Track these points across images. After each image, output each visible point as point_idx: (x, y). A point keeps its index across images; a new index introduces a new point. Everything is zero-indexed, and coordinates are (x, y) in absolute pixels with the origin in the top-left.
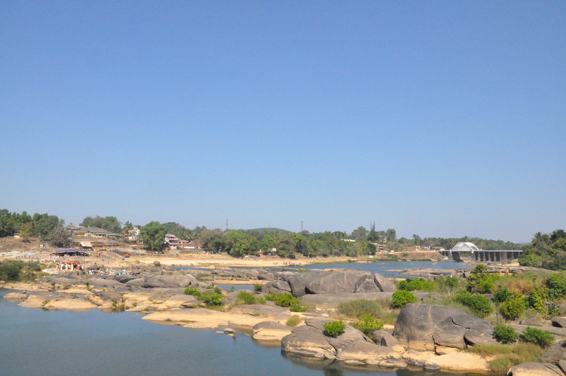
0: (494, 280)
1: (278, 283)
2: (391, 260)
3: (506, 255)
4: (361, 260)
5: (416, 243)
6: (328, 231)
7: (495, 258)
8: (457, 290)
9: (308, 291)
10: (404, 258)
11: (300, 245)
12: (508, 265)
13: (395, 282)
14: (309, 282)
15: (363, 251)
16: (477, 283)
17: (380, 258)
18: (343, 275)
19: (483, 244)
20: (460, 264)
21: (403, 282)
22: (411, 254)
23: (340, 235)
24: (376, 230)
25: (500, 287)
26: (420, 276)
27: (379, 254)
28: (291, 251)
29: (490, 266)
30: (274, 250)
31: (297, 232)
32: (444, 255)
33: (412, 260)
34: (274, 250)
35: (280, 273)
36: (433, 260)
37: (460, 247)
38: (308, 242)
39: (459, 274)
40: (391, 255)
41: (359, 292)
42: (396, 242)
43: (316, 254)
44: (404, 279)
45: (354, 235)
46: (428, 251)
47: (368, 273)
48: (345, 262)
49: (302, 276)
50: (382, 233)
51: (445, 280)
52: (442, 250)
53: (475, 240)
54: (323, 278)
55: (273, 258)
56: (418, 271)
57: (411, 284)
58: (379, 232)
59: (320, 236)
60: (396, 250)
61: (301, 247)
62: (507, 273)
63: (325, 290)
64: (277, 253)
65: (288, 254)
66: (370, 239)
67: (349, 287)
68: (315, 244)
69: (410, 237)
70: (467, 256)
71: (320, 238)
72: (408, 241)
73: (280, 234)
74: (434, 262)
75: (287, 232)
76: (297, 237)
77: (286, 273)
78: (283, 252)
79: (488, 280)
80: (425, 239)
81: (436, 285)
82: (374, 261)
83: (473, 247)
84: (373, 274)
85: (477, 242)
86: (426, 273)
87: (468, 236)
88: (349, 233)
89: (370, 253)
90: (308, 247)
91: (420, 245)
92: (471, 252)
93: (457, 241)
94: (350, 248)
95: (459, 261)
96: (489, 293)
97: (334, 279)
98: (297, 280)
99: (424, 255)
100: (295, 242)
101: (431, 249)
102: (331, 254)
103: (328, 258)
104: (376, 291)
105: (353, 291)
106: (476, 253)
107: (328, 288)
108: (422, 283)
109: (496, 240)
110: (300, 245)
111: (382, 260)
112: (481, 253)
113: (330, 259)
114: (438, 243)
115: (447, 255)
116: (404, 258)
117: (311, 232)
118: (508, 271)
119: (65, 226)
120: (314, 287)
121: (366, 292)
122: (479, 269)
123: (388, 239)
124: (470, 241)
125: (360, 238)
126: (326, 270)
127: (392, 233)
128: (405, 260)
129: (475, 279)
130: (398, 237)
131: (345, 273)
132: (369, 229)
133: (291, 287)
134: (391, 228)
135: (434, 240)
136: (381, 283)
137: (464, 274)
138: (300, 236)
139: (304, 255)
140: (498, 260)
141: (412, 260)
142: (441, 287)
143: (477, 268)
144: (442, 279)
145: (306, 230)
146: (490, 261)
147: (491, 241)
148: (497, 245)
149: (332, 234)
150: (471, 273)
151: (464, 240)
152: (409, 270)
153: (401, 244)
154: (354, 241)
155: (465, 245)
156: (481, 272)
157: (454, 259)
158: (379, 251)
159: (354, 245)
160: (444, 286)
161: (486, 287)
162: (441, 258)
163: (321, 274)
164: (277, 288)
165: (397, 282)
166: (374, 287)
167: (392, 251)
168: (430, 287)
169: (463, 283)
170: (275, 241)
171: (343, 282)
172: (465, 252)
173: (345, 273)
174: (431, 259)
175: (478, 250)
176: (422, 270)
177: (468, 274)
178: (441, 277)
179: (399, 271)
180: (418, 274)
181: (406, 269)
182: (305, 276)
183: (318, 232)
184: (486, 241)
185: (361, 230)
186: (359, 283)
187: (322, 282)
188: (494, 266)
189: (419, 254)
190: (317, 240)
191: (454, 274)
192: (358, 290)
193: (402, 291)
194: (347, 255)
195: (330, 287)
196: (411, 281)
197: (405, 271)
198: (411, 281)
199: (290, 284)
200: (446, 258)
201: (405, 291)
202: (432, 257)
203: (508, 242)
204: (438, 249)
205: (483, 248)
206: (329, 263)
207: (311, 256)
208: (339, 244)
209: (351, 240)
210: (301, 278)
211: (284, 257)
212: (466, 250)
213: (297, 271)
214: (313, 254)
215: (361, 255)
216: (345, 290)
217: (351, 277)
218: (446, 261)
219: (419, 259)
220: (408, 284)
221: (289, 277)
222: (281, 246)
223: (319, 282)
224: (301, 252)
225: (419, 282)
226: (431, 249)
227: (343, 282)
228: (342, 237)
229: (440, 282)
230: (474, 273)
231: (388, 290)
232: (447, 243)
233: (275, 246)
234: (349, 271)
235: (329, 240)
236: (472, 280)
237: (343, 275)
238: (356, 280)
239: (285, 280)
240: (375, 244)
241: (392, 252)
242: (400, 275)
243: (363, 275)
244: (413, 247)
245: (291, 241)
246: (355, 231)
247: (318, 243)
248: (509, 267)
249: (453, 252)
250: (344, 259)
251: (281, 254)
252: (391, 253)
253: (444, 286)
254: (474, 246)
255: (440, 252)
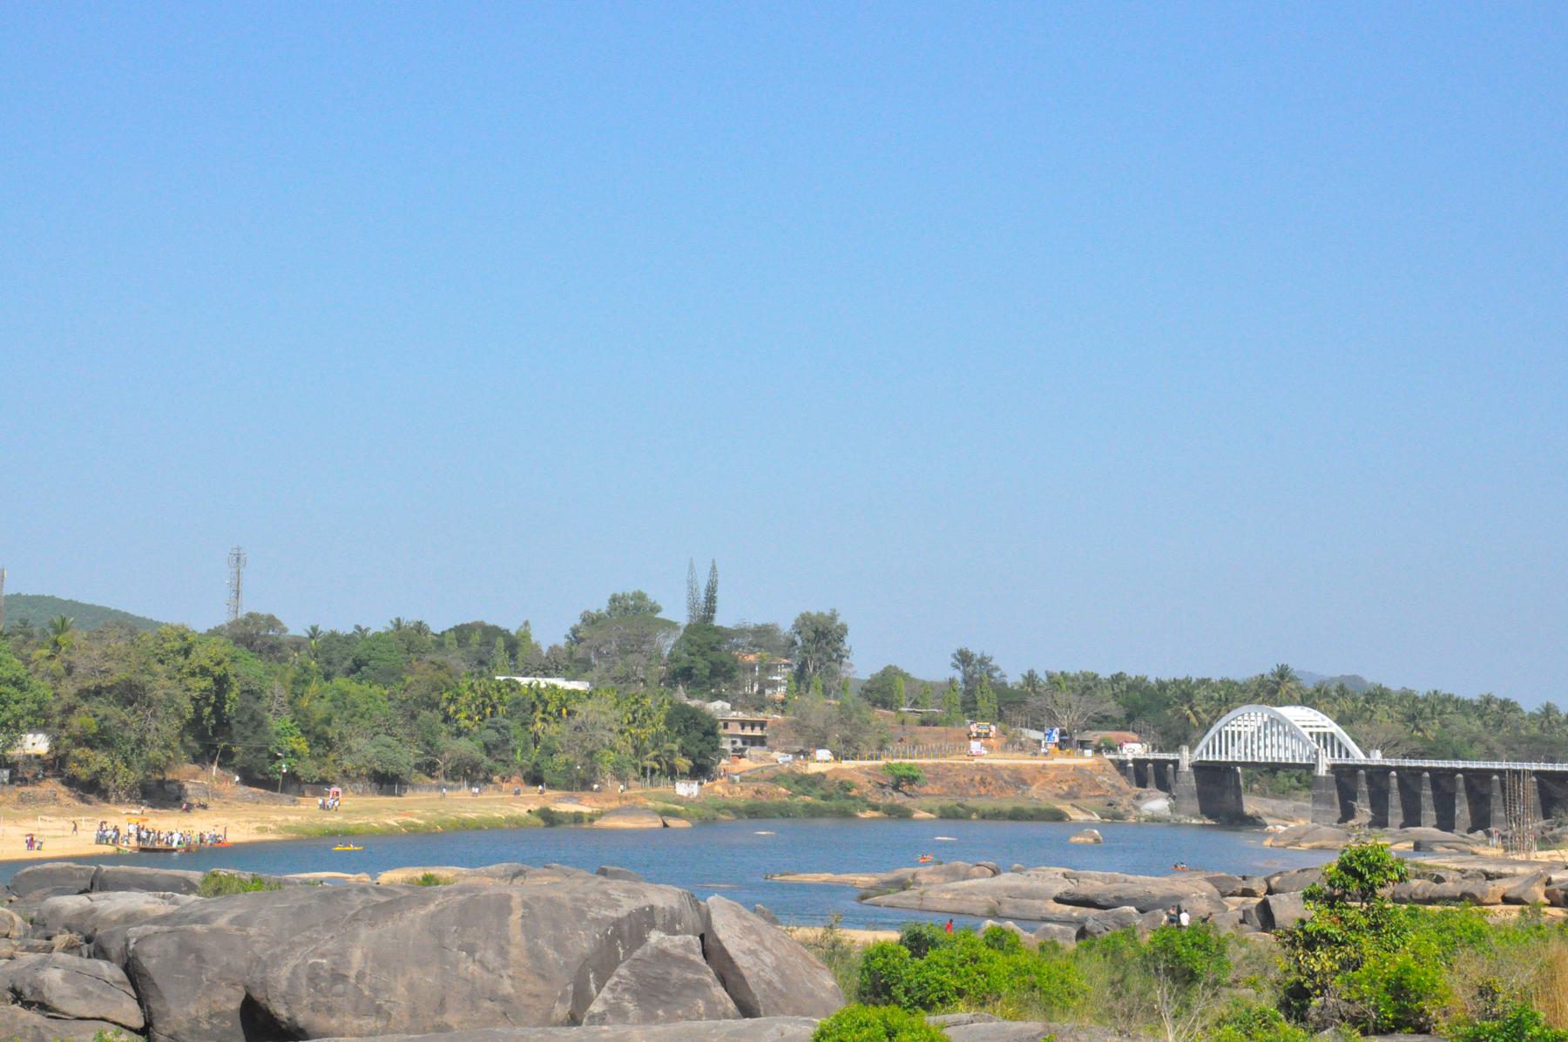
0: (1449, 950)
1: (53, 976)
2: (813, 812)
3: (1530, 789)
4: (622, 807)
5: (970, 707)
6: (410, 618)
7: (1462, 810)
8: (1220, 1009)
9: (883, 786)
10: (898, 799)
11: (217, 709)
12: (1543, 856)
13: (834, 954)
14: (275, 960)
15: (639, 751)
16: (1346, 965)
17: (742, 795)
18: (502, 906)
19: (1386, 721)
20: (1244, 839)
21: (882, 951)
22: (938, 774)
23: (488, 645)
24: (722, 619)
25: (1486, 991)
26: (993, 914)
27: (742, 771)
28: (154, 753)
29: (1428, 861)
30: (37, 744)
31: (200, 623)
32: (1142, 783)
33: (948, 815)
34: (37, 744)
35: (72, 903)
36: (1078, 816)
37: (1247, 735)
38: (278, 689)
39: (1234, 904)
40: (814, 781)
41: (601, 1019)
42: (850, 697)
43: (331, 772)
44: (891, 936)
45: (580, 652)
46: (1044, 760)
47: (664, 897)
48: (517, 824)
49: (221, 922)
50: (763, 636)
51: (1146, 939)
52: (1134, 750)
53: (1342, 690)
54: (364, 933)
55: (23, 800)
56: (981, 887)
57: (933, 968)
58: (741, 632)
59: (359, 650)
60: (847, 749)
61: (223, 725)
62: (1536, 908)
63: (378, 1011)
64: (54, 766)
65: (135, 776)
66: (683, 675)
67: (539, 987)
68: (320, 709)
69: (936, 668)
70: (1283, 794)
71: (357, 666)
72: (921, 693)
73: (78, 636)
74: (1080, 827)
75: (129, 626)
76: (200, 657)
77: (114, 903)
78: (101, 759)
79: (1413, 950)
80: (1030, 679)
81: (1091, 975)
82: (707, 818)
83: (1327, 739)
84: (695, 903)
85: (1351, 702)
86: (1031, 895)
87: (1296, 666)
88: (550, 635)
89: (683, 763)
90: (275, 724)
91: (1000, 717)
92: (1310, 768)
93: (1229, 696)
94: (552, 729)
95: (1240, 821)
96: (1421, 1030)
97: (439, 933)
98: (189, 948)
99: (1019, 779)
100: (177, 692)
101: (1063, 744)
102: (429, 768)
103: (410, 796)
104: (713, 1013)
105: (561, 1011)
106: (1345, 775)
107: (399, 996)
108: (1000, 963)
109: (1472, 693)
110: (217, 709)
111: (754, 812)
112: (1377, 775)
113: (420, 807)
114: (1112, 708)
115: (1163, 785)
116: (898, 799)
117: (296, 627)
118: (1539, 892)
119: (545, 650)
120: (304, 990)
121: (649, 1018)
122: (1359, 875)
123: (800, 676)
124: (1306, 701)
125: (619, 669)
126: (386, 877)
127: (822, 638)
128: (902, 814)
129: (1329, 940)
130: (862, 662)
131: (517, 893)
132: (676, 610)
133: (140, 1001)
134: (818, 606)
135: (1087, 685)
136: (743, 962)
137: (1265, 910)
138: (223, 649)
139: (248, 779)
140: (1481, 822)
141: (948, 815)
142: (1118, 987)
143: (1346, 868)
144: (1129, 932)
145: (263, 610)
146: (1428, 830)
147: (1441, 704)
148: (1476, 725)
149: (440, 642)
150: (1309, 896)
151: (1274, 689)
152: (924, 874)
153: (879, 711)
154: (580, 686)
155: (1274, 721)
156: (1368, 893)
157: (1206, 811)
158: (740, 754)
159: (583, 710)
160: (1136, 981)
161: (1398, 989)
162: (1124, 803)
163: (358, 901)
164: (44, 1007)
165: (845, 955)
166: (699, 987)
167: (823, 754)
168: (1053, 987)
169: (1258, 962)
170: (42, 688)
171: (502, 952)
172: (1273, 768)
173: (517, 893)
174: (1065, 807)
175: (1358, 756)
176: (1006, 879)
177: (1288, 909)
178: (1123, 923)
179: (864, 879)
180: (980, 903)
181: (905, 872)
182: (241, 922)
183: (346, 629)
184: (1405, 695)
185: (632, 615)
186: (603, 962)
187: (357, 956)
188: (1455, 857)
189: (987, 777)
190: (340, 682)
191: (1204, 907)
192: (596, 1008)
193: (873, 1014)
194: (535, 778)
195: (411, 987)
196: (933, 943)
197: (902, 885)
198: (933, 943)
199: (134, 973)
200: (1157, 804)
201: (895, 1015)
202: (1071, 796)
203: (1548, 710)
204: (1111, 748)
205: (1388, 747)
206: (414, 832)
207: (292, 784)
208: (485, 706)
209: (561, 683)
210: (215, 932)
211: (104, 795)
212: (1284, 756)
213: (190, 887)
214: (308, 769)
215: (621, 777)
216: (509, 1010)
217: (556, 925)
218: (1154, 819)
219: (987, 805)
220: (912, 970)
221: (135, 931)
222: (82, 721)
223: (342, 956)
224: (226, 759)
225: (984, 951)
226: (1063, 744)
227: (502, 952)
228: (501, 657)
229: (1113, 953)
230: (1331, 901)
231: (790, 1001)
232: (1164, 709)
233: (40, 720)
234: (542, 883)
235: (418, 678)
236: (1310, 943)
237: (502, 906)
238: (584, 942)
239: (101, 953)
240: (718, 707)
241: (822, 762)
242: (865, 907)
243: (628, 906)
244: (955, 731)
245: (160, 685)
246: (591, 621)
247: (341, 701)
248: (1552, 866)
249: (1200, 768)
250: (508, 803)
251: (84, 773)
252: (813, 768)
253: (1136, 981)
254: (1333, 727)
255: (1121, 766)
